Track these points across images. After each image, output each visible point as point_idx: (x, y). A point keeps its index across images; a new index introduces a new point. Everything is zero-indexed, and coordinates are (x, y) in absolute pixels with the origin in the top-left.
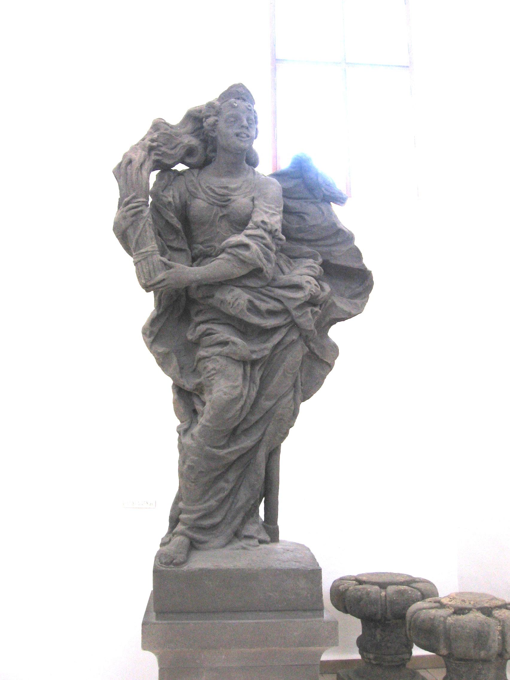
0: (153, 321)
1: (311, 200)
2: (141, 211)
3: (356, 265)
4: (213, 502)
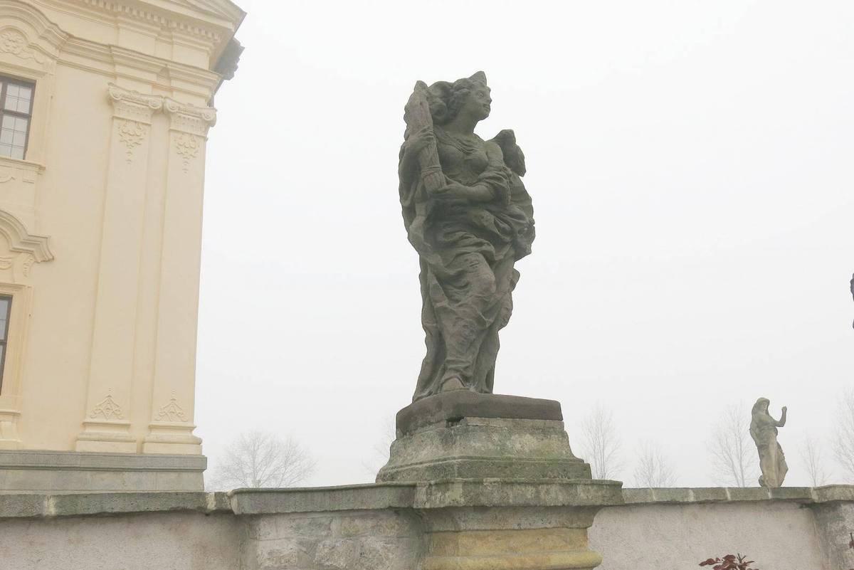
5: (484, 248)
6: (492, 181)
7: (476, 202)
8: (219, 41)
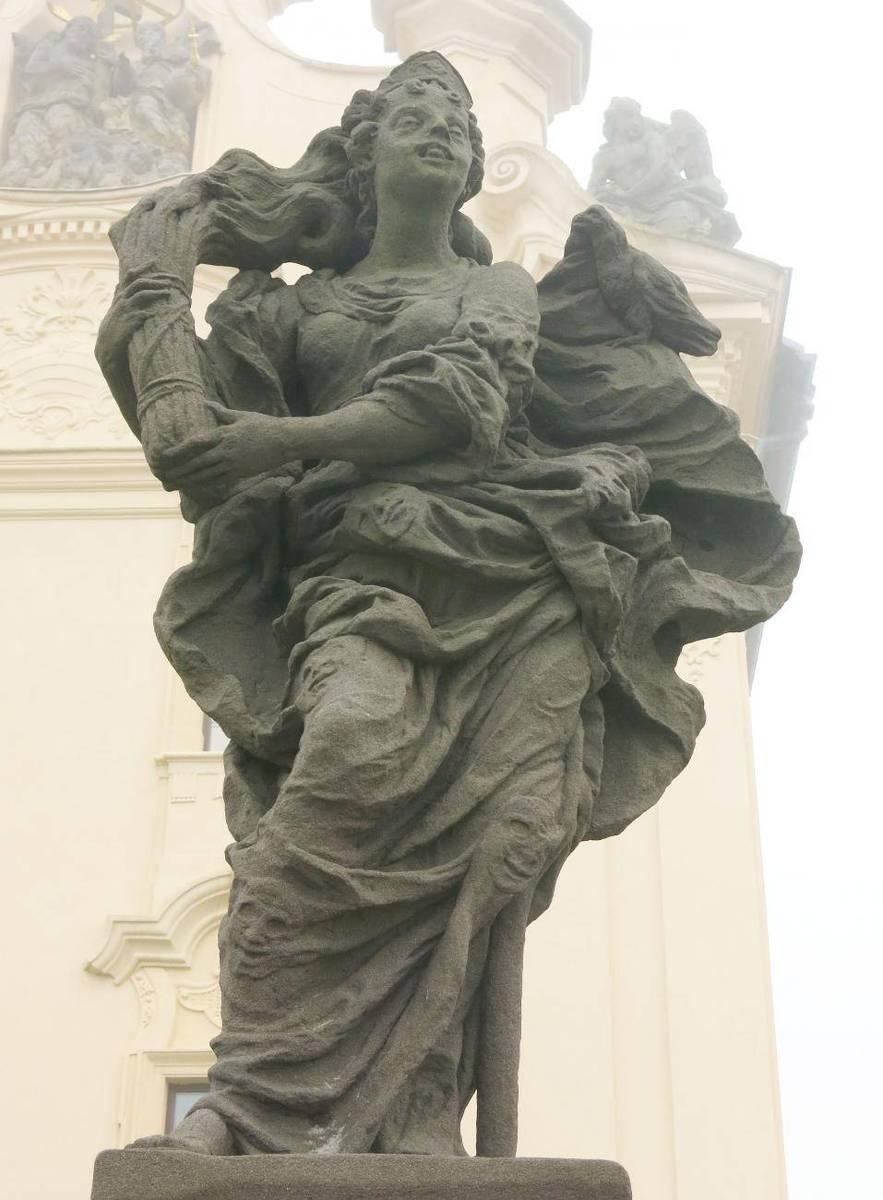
0: (182, 584)
1: (622, 340)
2: (166, 297)
3: (751, 492)
4: (320, 1031)
5: (378, 611)
6: (394, 380)
7: (379, 463)
8: (738, 356)
